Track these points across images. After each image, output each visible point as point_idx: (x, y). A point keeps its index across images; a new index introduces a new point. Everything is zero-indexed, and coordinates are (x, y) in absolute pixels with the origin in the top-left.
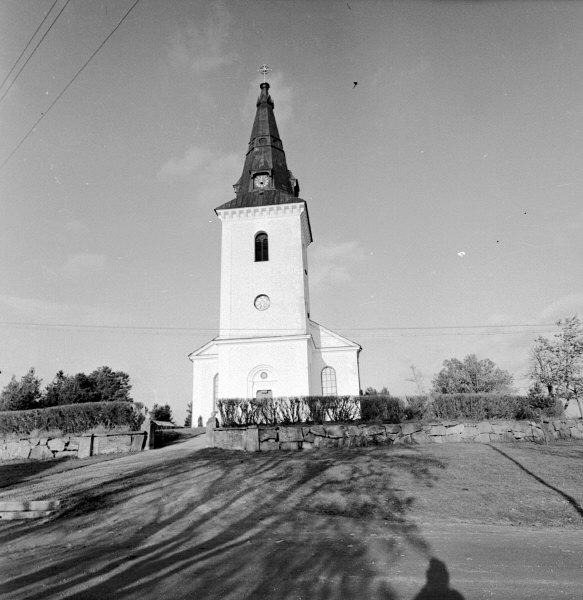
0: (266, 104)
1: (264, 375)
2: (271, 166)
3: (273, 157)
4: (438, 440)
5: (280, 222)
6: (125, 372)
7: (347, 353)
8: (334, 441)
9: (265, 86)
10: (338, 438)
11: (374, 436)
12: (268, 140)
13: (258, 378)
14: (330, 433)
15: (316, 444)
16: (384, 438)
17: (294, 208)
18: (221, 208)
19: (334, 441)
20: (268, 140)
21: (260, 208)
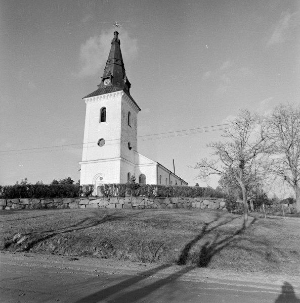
0: (116, 42)
1: (101, 179)
2: (112, 74)
3: (115, 69)
4: (83, 207)
5: (114, 101)
6: (91, 183)
7: (152, 167)
8: (22, 206)
9: (117, 33)
10: (25, 205)
11: (46, 204)
12: (117, 60)
13: (98, 180)
14: (22, 202)
15: (13, 207)
16: (51, 205)
17: (118, 93)
18: (85, 97)
19: (22, 206)
20: (117, 60)
21: (102, 95)
